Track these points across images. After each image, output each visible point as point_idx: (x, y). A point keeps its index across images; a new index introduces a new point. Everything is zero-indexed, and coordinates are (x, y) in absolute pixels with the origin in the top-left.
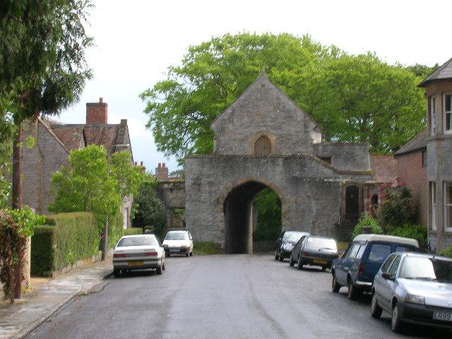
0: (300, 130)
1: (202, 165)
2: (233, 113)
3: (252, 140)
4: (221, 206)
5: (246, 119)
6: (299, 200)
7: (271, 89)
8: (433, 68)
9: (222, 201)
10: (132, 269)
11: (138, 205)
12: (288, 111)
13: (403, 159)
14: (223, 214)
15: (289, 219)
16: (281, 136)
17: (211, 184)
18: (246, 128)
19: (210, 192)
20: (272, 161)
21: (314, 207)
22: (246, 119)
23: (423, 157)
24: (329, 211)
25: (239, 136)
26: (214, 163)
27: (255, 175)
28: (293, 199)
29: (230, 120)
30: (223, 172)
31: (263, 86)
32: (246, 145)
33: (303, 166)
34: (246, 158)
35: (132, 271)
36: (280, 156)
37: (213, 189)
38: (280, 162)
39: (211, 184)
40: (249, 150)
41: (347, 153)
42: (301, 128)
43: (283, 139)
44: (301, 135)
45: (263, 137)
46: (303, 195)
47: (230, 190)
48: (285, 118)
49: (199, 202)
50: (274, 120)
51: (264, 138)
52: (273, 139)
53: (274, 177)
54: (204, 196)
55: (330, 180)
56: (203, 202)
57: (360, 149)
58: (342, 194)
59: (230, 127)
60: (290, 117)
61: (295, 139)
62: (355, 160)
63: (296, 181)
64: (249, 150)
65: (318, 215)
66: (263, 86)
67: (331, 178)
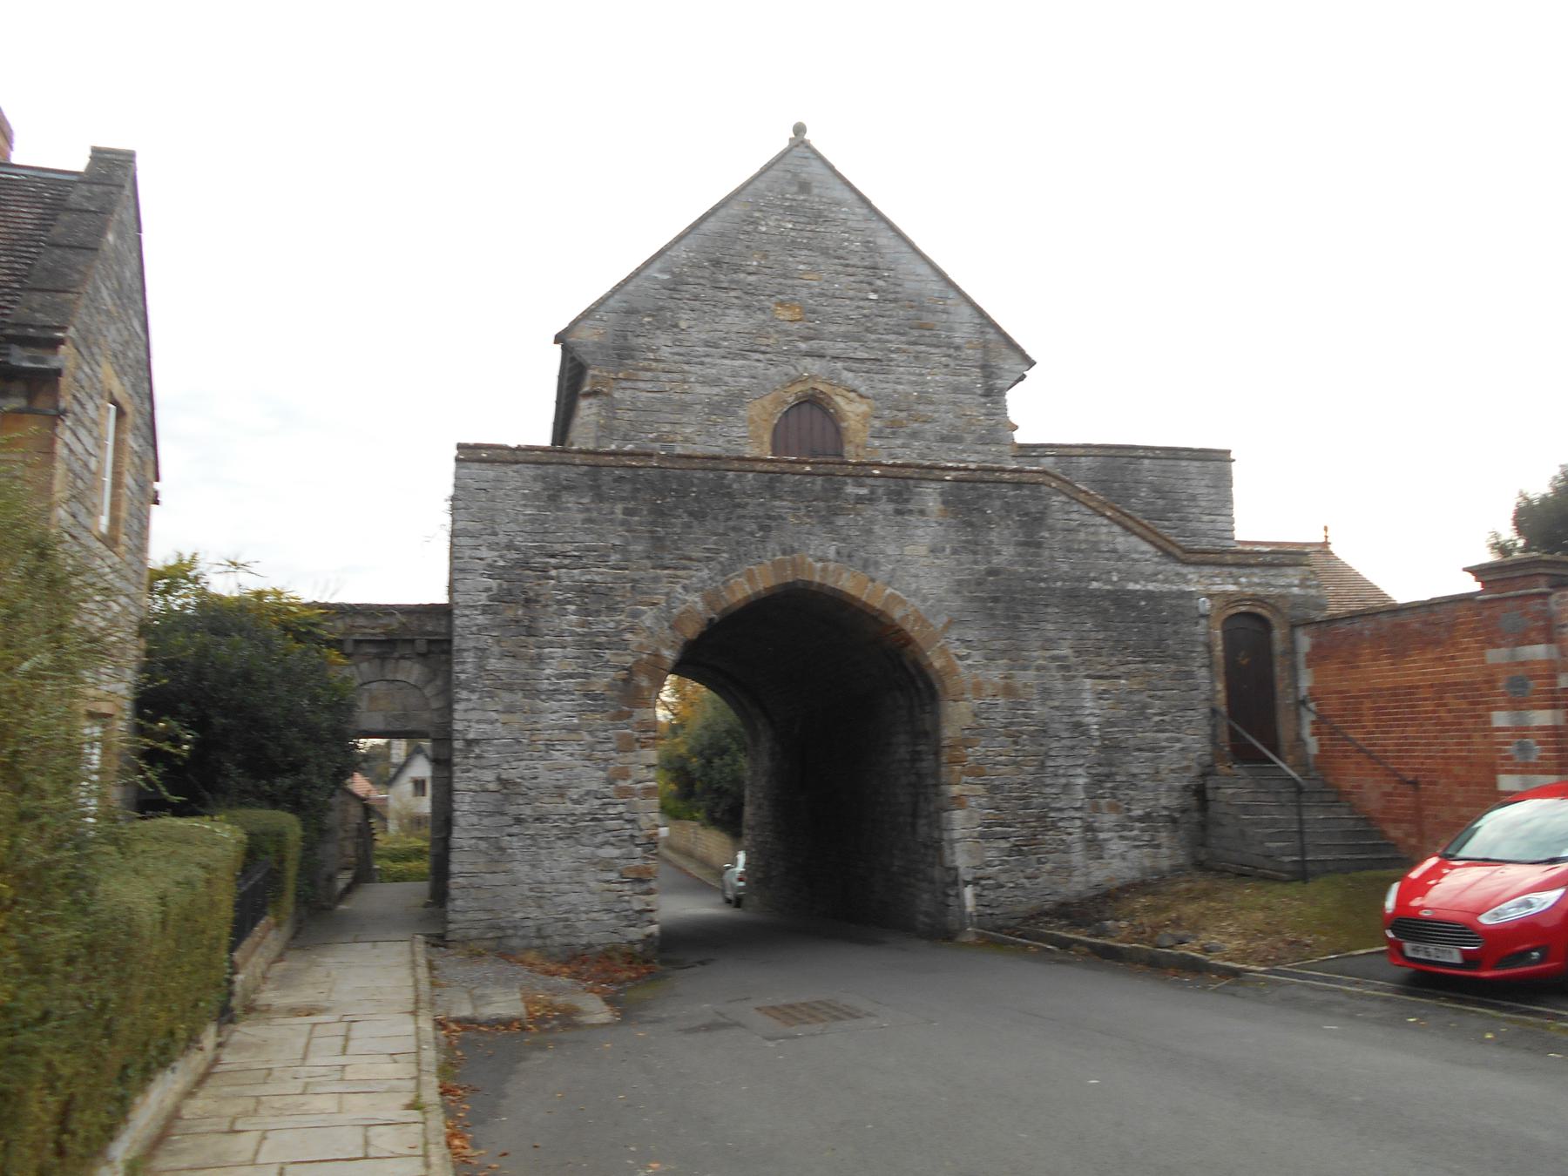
7: (839, 204)
8: (1002, 392)
18: (734, 357)
35: (1131, 586)
36: (930, 472)
37: (607, 623)
38: (930, 497)
39: (592, 598)
40: (748, 434)
43: (898, 418)
44: (974, 407)
46: (1038, 656)
47: (692, 631)
49: (534, 693)
51: (814, 403)
52: (852, 410)
54: (558, 661)
58: (1209, 647)
64: (748, 434)
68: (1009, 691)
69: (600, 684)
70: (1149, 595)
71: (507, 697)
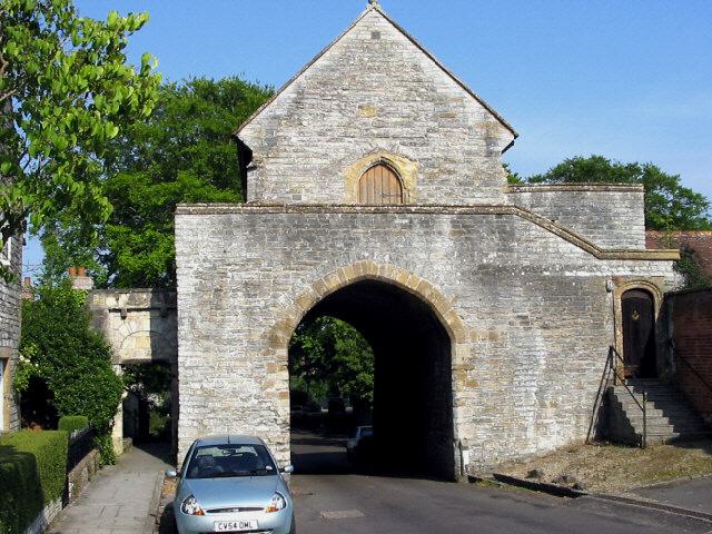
0: (475, 148)
1: (227, 232)
2: (298, 103)
3: (352, 171)
4: (283, 352)
5: (335, 117)
6: (500, 329)
9: (284, 338)
10: (239, 446)
11: (32, 349)
12: (440, 100)
13: (516, 131)
14: (285, 374)
15: (472, 384)
16: (428, 163)
17: (250, 288)
18: (337, 140)
19: (250, 312)
20: (424, 223)
21: (541, 344)
22: (335, 117)
23: (390, 169)
24: (581, 358)
25: (317, 162)
26: (261, 228)
27: (383, 263)
28: (483, 327)
29: (292, 118)
30: (288, 255)
31: (376, 35)
32: (337, 186)
33: (507, 236)
34: (351, 214)
35: (567, 274)
38: (445, 223)
39: (250, 288)
41: (594, 210)
42: (478, 145)
43: (434, 170)
45: (384, 164)
48: (435, 118)
50: (408, 122)
52: (407, 170)
53: (429, 267)
54: (234, 323)
55: (581, 274)
56: (230, 342)
57: (623, 199)
59: (292, 134)
60: (448, 116)
61: (464, 171)
62: (610, 227)
63: (489, 278)
64: (343, 191)
65: (553, 371)
66: (376, 35)
67: (580, 268)
68: (493, 337)
69: (256, 337)
70: (577, 279)
71: (206, 343)
